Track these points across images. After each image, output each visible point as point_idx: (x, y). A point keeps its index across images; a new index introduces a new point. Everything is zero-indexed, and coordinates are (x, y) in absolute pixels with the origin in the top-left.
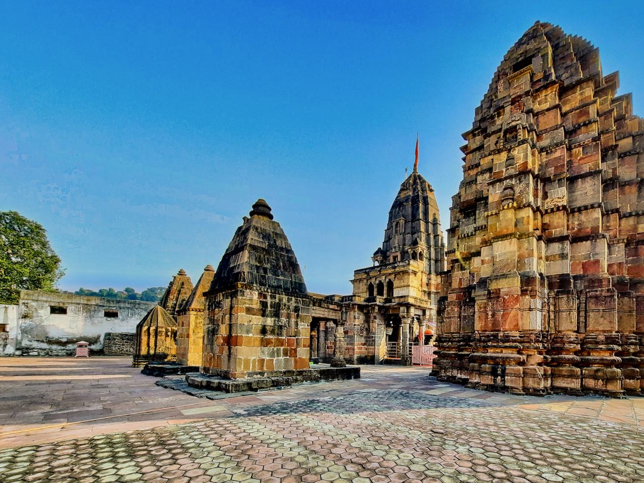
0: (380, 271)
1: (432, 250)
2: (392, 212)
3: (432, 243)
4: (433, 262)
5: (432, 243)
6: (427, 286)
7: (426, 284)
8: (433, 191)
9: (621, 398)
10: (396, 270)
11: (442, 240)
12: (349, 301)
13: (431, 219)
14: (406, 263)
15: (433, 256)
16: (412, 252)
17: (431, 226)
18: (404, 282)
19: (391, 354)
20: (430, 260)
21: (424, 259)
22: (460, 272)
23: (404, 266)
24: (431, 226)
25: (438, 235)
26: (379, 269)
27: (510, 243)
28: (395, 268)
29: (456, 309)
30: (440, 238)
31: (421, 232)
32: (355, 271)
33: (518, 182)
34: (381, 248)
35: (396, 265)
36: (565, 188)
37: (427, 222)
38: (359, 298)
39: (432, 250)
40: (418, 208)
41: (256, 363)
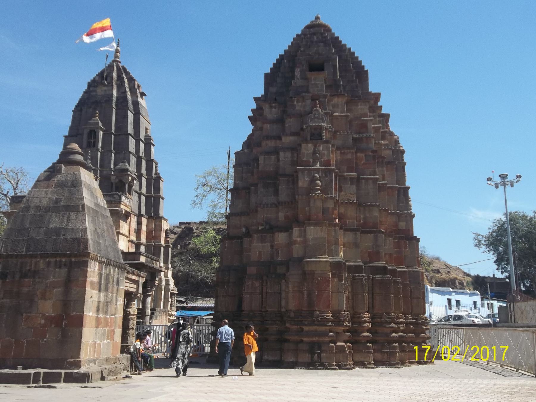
1: (144, 181)
2: (81, 110)
3: (144, 171)
4: (143, 198)
5: (144, 171)
8: (145, 95)
9: (443, 358)
11: (156, 167)
13: (142, 136)
14: (114, 198)
15: (144, 190)
16: (117, 180)
17: (142, 145)
19: (169, 333)
20: (140, 195)
21: (134, 193)
22: (260, 244)
24: (142, 145)
25: (153, 160)
27: (321, 230)
29: (257, 284)
30: (154, 165)
31: (130, 153)
33: (324, 175)
36: (355, 186)
37: (138, 141)
39: (144, 181)
40: (126, 117)
41: (396, 333)
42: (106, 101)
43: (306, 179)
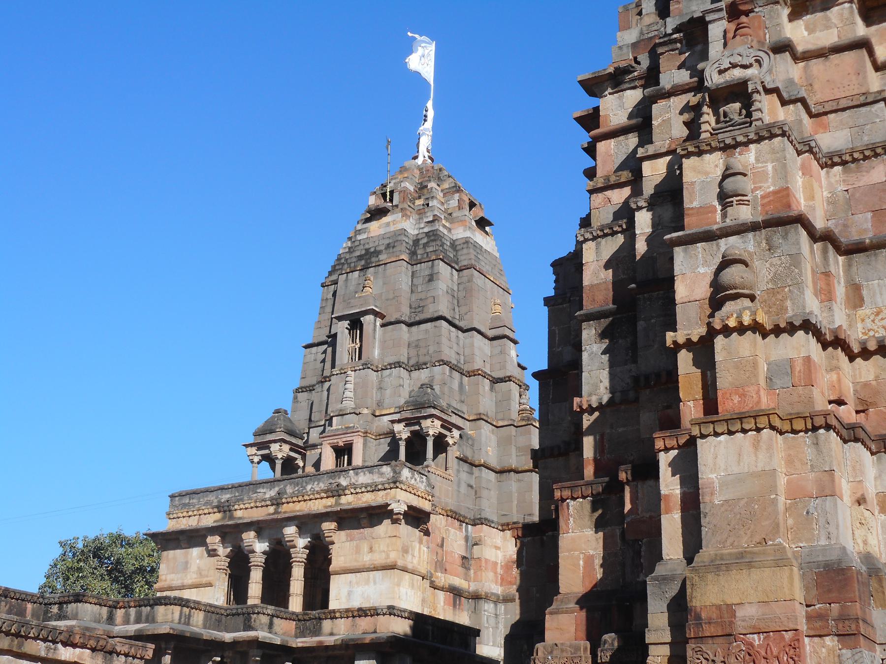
0: (277, 502)
6: (461, 570)
7: (459, 561)
8: (489, 224)
10: (344, 500)
12: (138, 621)
18: (371, 549)
23: (374, 488)
26: (272, 493)
28: (337, 492)
32: (172, 497)
34: (286, 412)
35: (344, 482)
38: (186, 610)
42: (388, 246)
43: (702, 270)
